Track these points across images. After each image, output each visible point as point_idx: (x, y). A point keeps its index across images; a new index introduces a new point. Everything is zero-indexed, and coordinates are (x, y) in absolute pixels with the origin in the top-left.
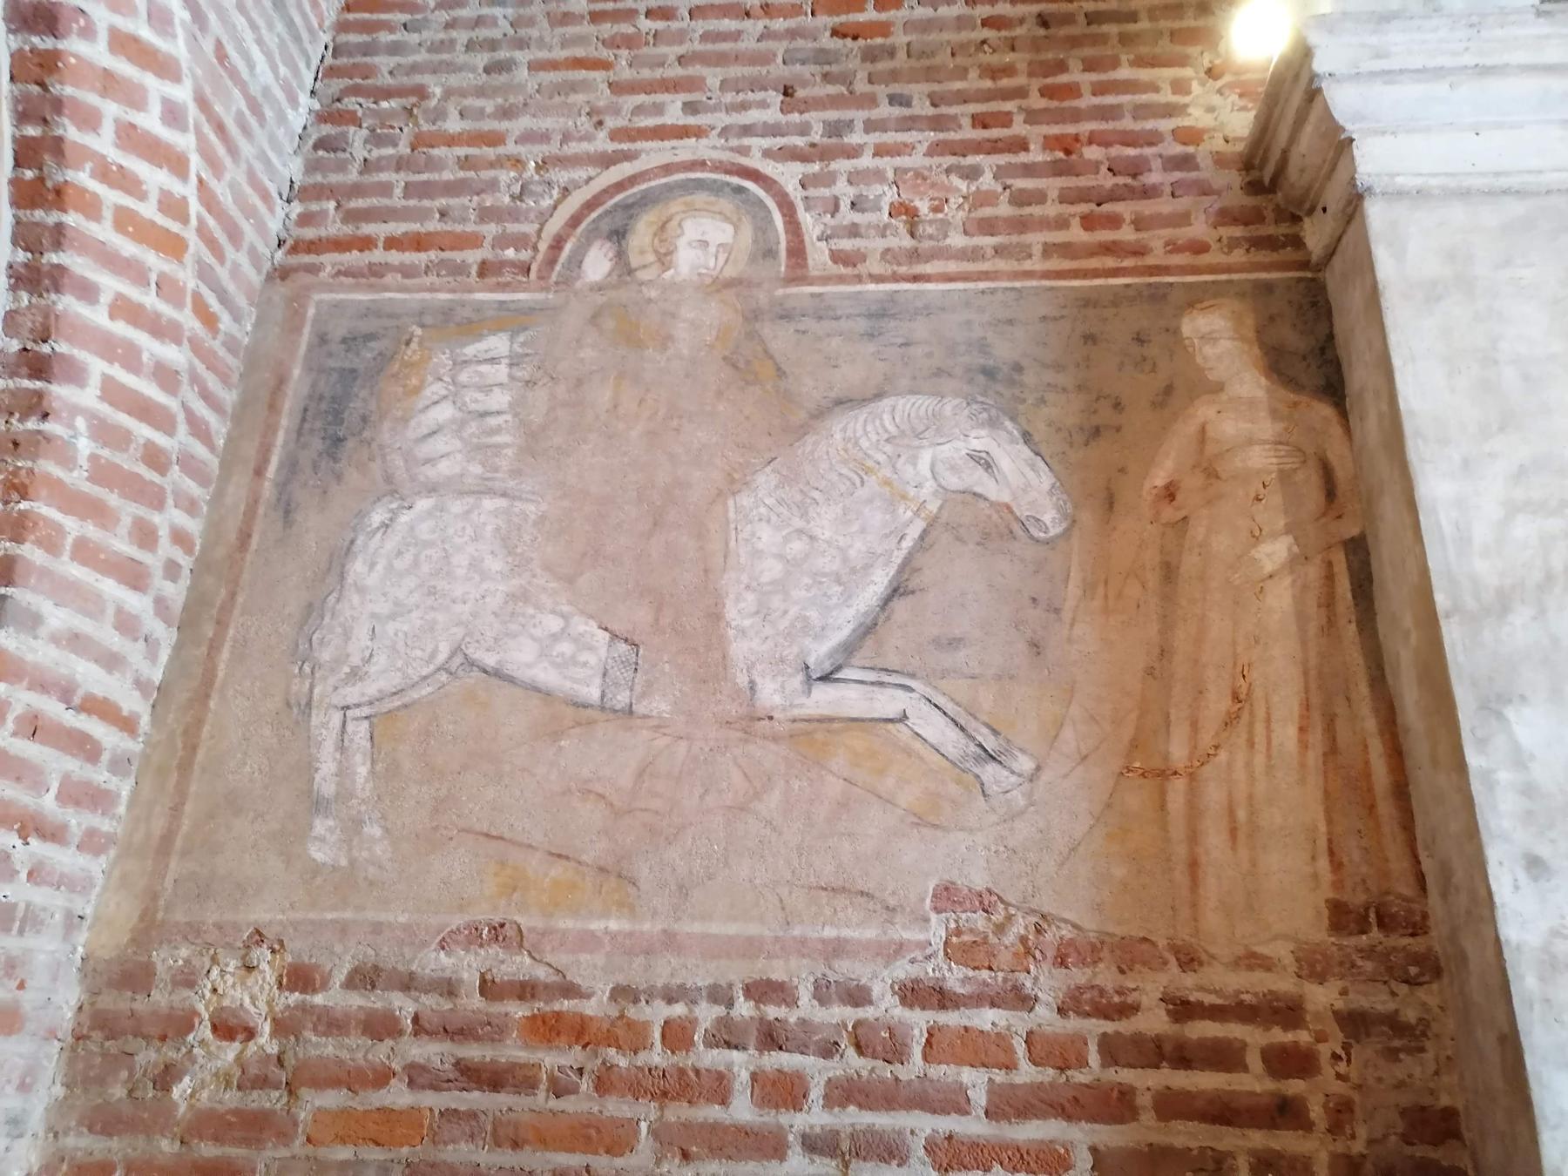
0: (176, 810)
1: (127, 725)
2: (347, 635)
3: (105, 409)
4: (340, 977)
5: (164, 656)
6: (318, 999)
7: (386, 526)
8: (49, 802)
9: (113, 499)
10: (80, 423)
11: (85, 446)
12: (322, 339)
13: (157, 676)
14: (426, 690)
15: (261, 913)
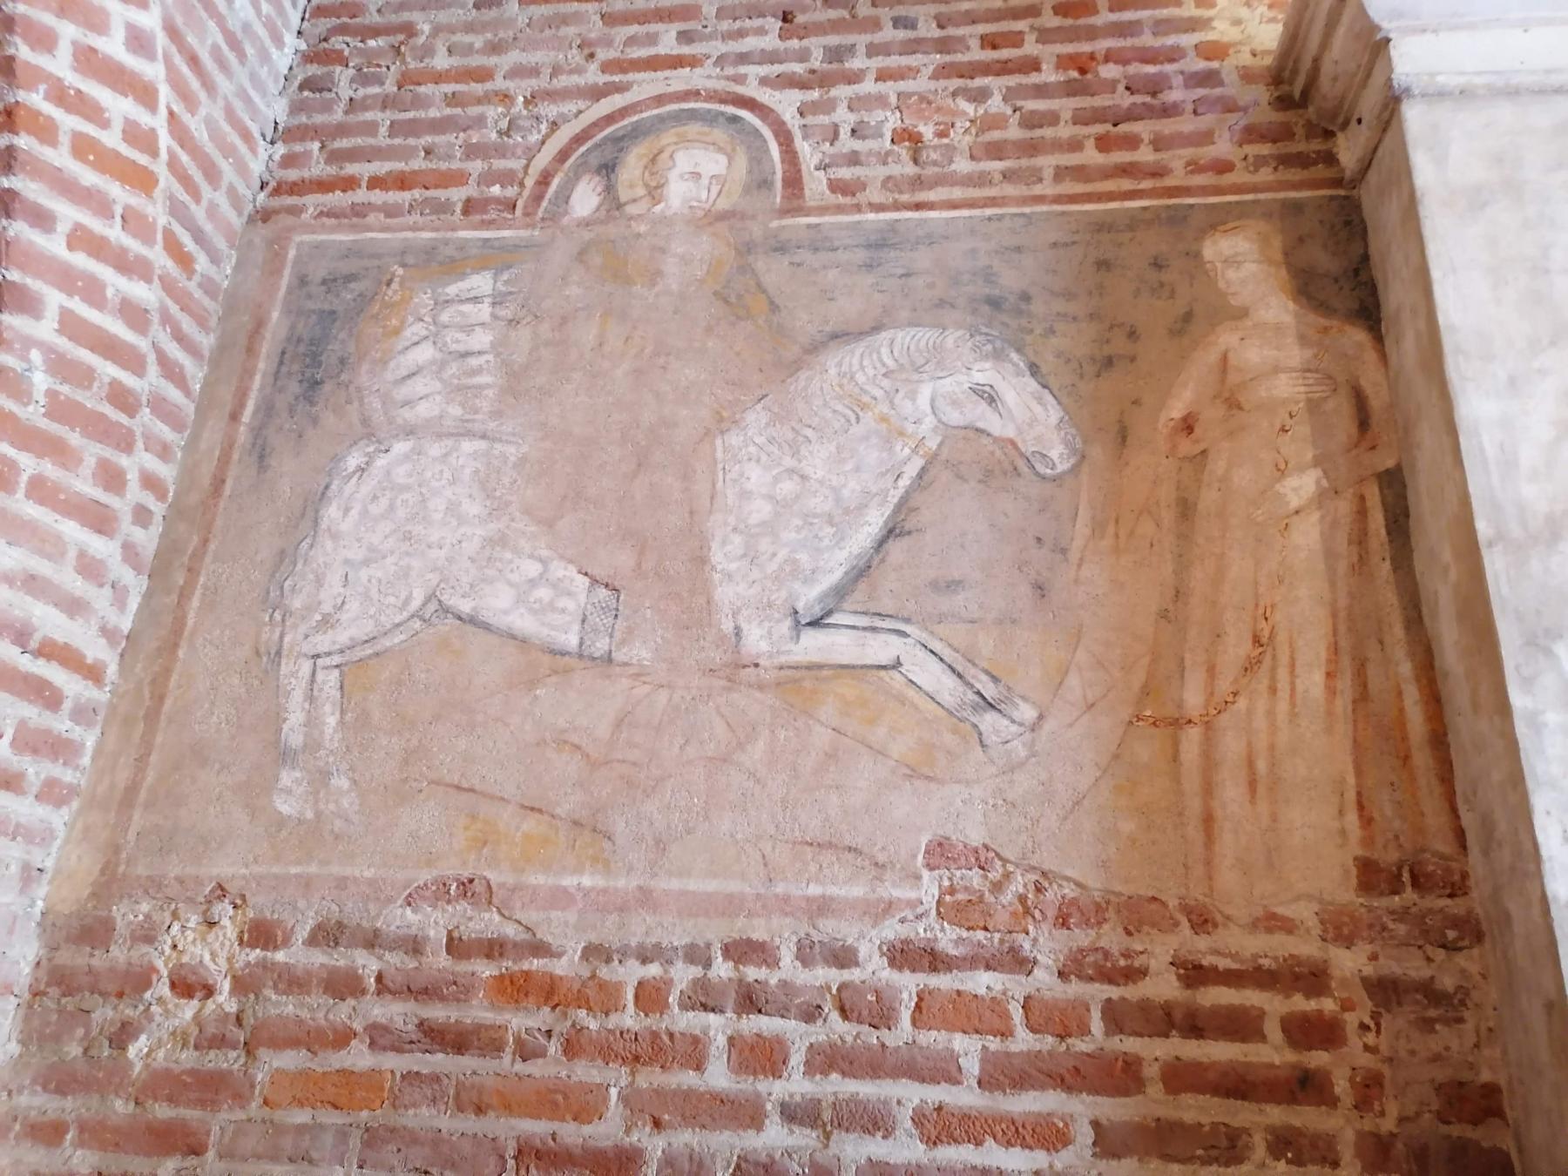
0: (142, 761)
1: (93, 673)
2: (319, 582)
3: (63, 343)
4: (302, 933)
5: (134, 603)
6: (280, 956)
7: (361, 470)
9: (74, 438)
10: (35, 355)
11: (41, 381)
12: (302, 281)
13: (126, 624)
14: (398, 638)
15: (224, 867)
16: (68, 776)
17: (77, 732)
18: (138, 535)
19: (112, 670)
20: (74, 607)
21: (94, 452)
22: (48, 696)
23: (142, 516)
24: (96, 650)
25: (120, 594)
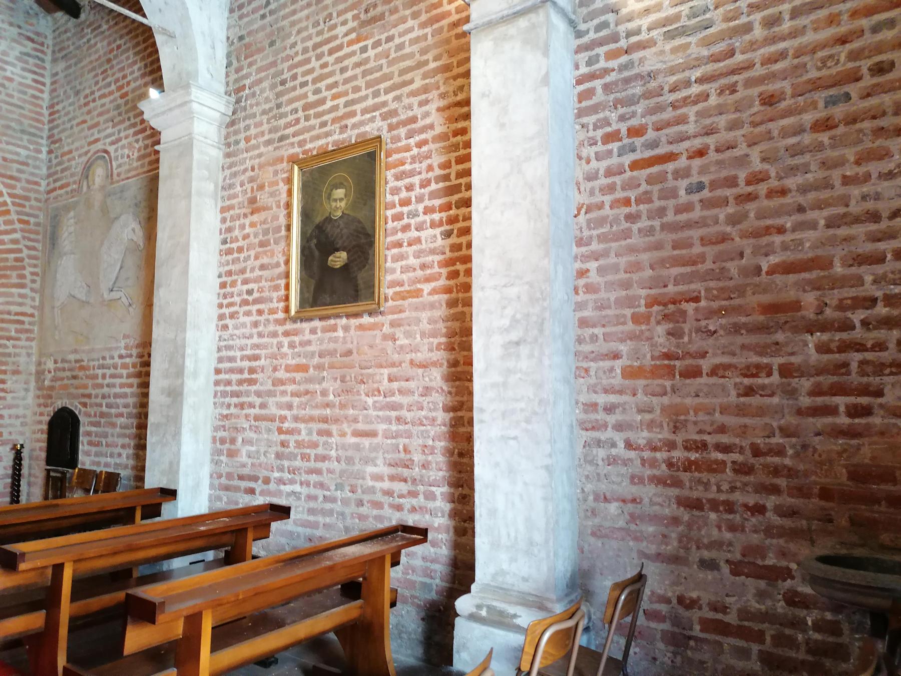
1: (32, 315)
5: (37, 300)
8: (13, 334)
9: (8, 272)
13: (37, 304)
16: (32, 336)
17: (31, 327)
18: (34, 286)
19: (36, 314)
20: (20, 304)
21: (14, 274)
22: (23, 323)
23: (33, 281)
24: (29, 311)
25: (33, 299)
